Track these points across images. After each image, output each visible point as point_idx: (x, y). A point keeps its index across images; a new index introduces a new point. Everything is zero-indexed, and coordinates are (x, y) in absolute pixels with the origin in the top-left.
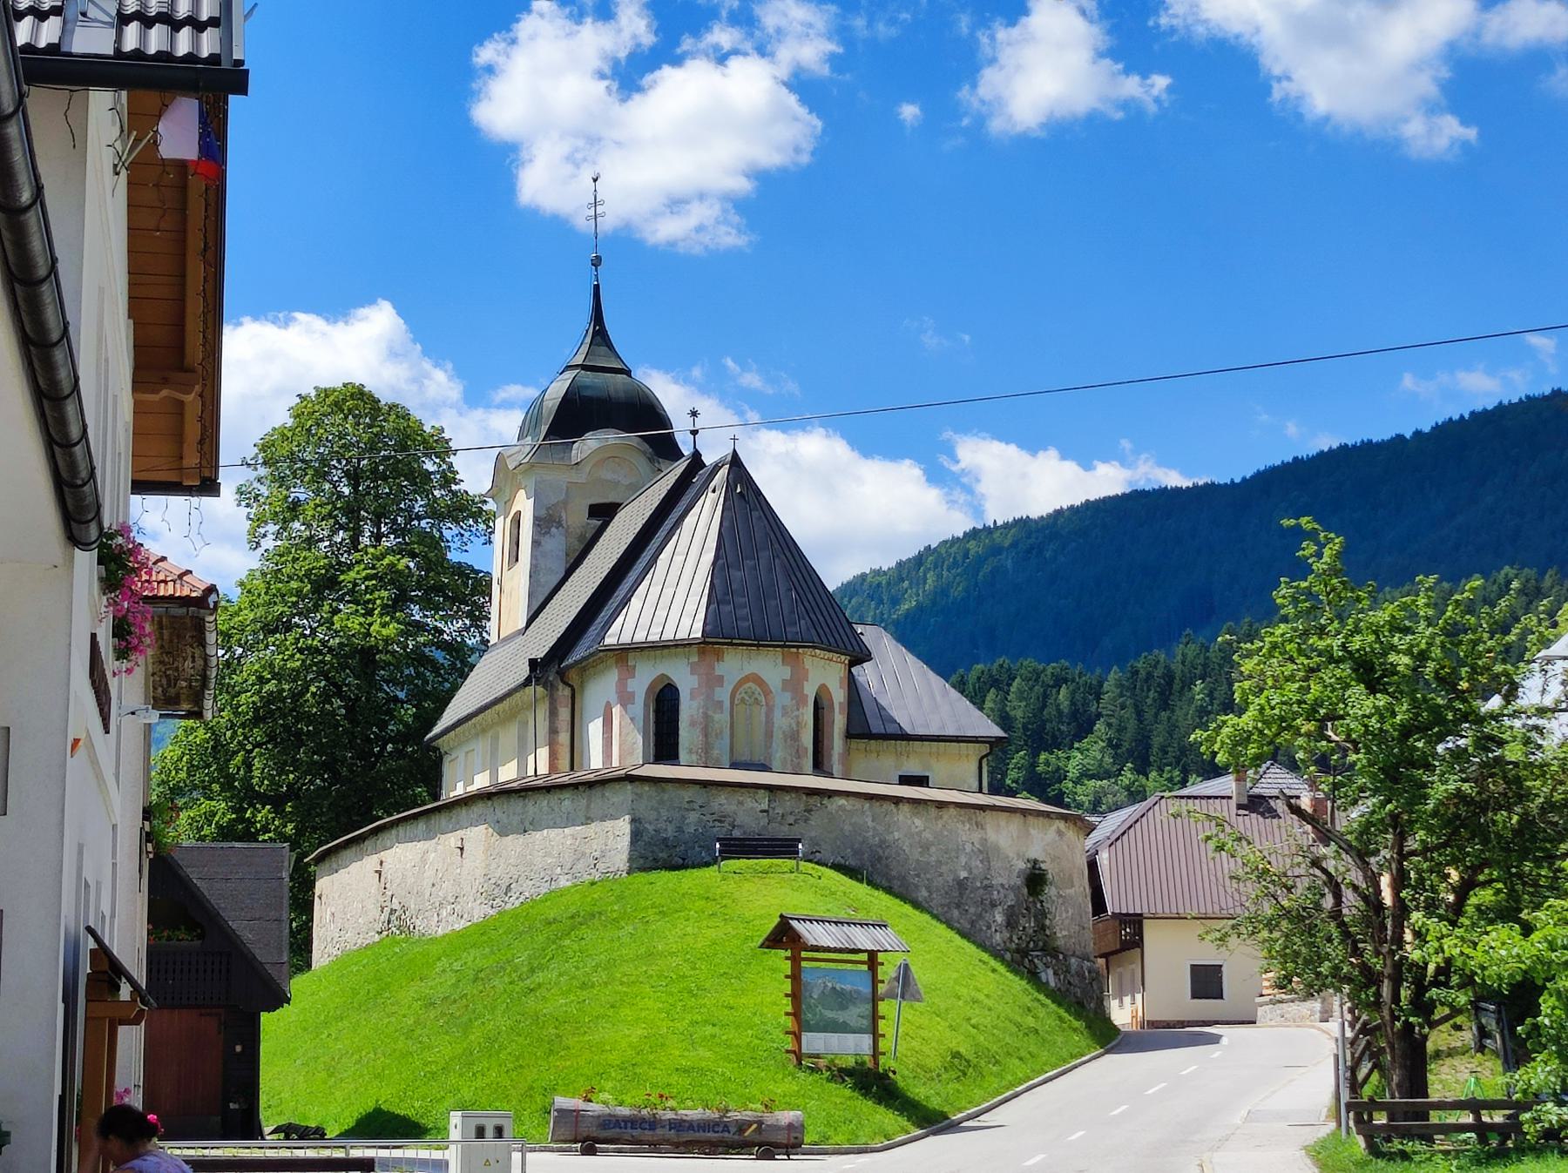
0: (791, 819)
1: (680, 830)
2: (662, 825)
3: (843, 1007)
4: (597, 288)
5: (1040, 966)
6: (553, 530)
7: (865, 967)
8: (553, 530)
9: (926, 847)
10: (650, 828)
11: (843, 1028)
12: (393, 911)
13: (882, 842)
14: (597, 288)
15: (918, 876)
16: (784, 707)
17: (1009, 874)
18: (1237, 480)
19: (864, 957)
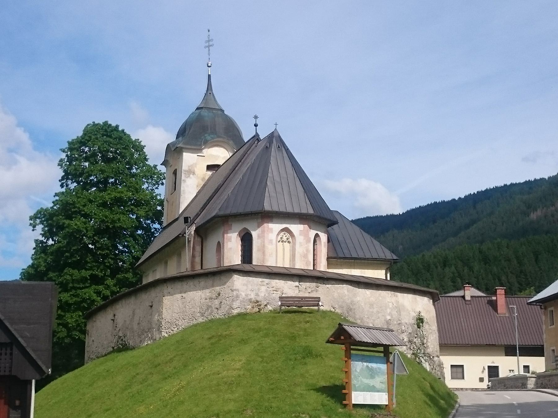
0: (310, 290)
1: (257, 295)
2: (249, 293)
3: (372, 377)
4: (209, 76)
5: (423, 361)
6: (191, 176)
7: (382, 355)
8: (191, 176)
9: (372, 305)
10: (243, 294)
11: (372, 389)
12: (120, 337)
13: (352, 301)
14: (209, 76)
15: (368, 318)
16: (300, 243)
17: (409, 319)
18: (401, 214)
19: (381, 349)
